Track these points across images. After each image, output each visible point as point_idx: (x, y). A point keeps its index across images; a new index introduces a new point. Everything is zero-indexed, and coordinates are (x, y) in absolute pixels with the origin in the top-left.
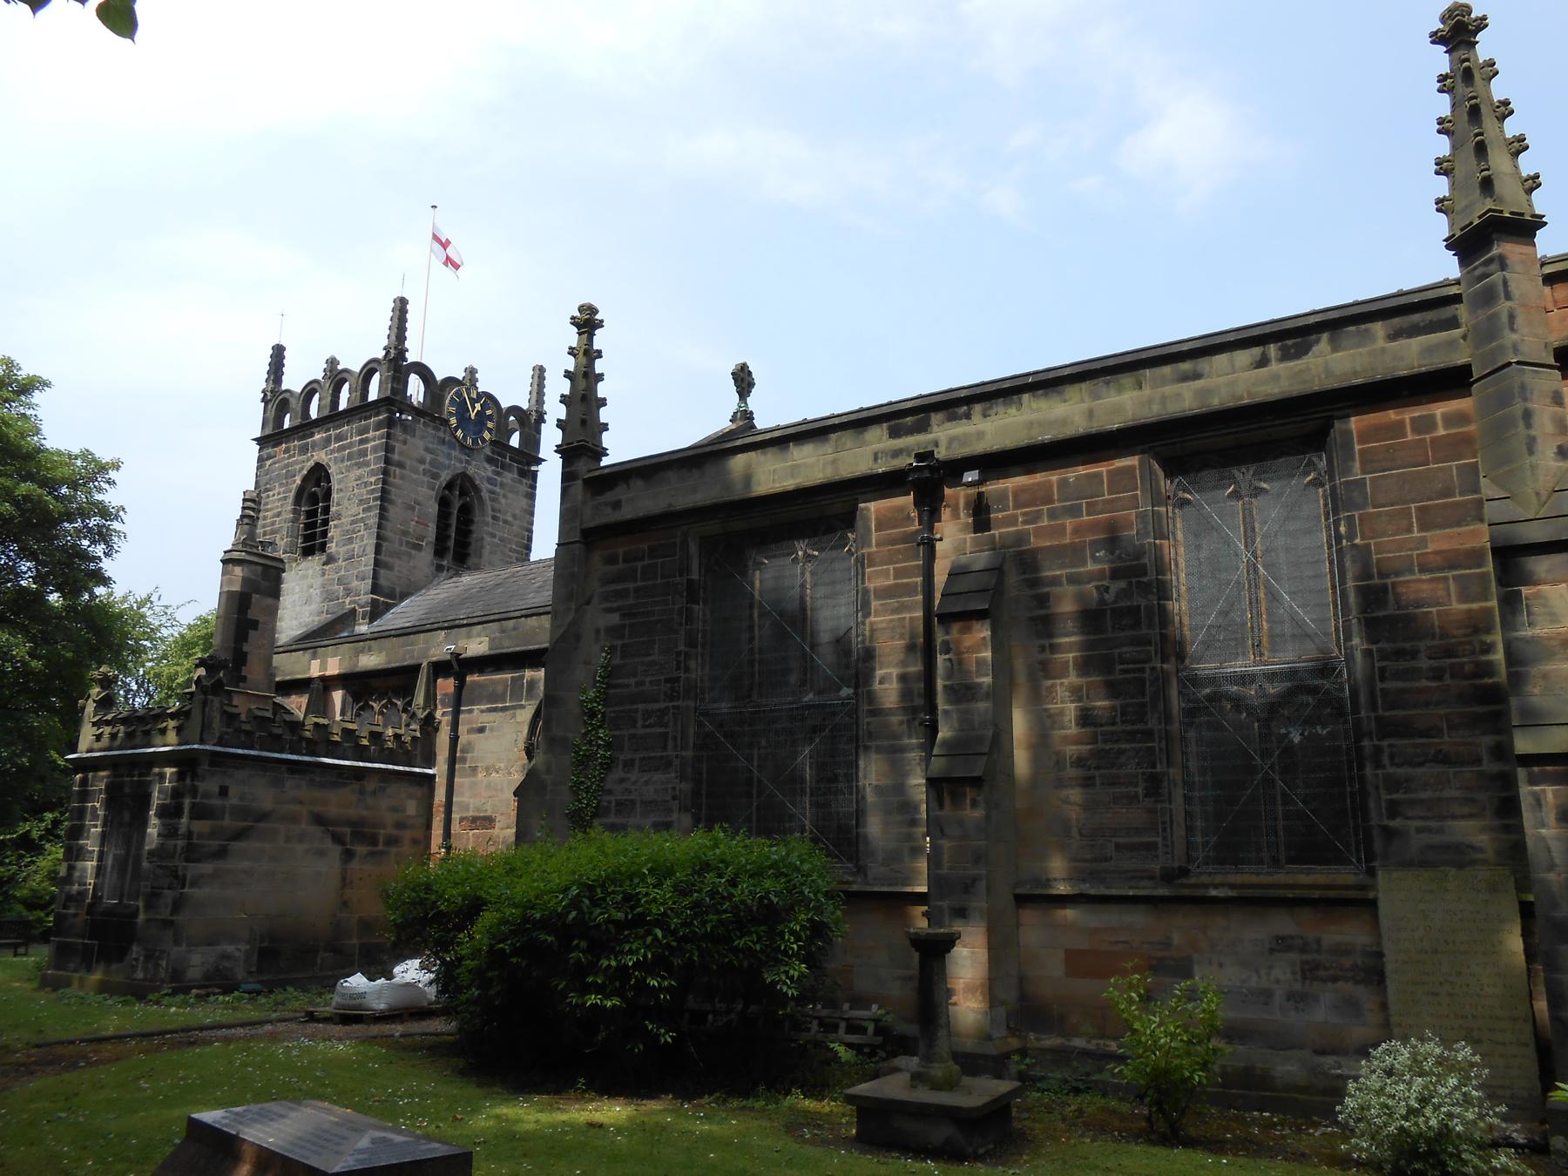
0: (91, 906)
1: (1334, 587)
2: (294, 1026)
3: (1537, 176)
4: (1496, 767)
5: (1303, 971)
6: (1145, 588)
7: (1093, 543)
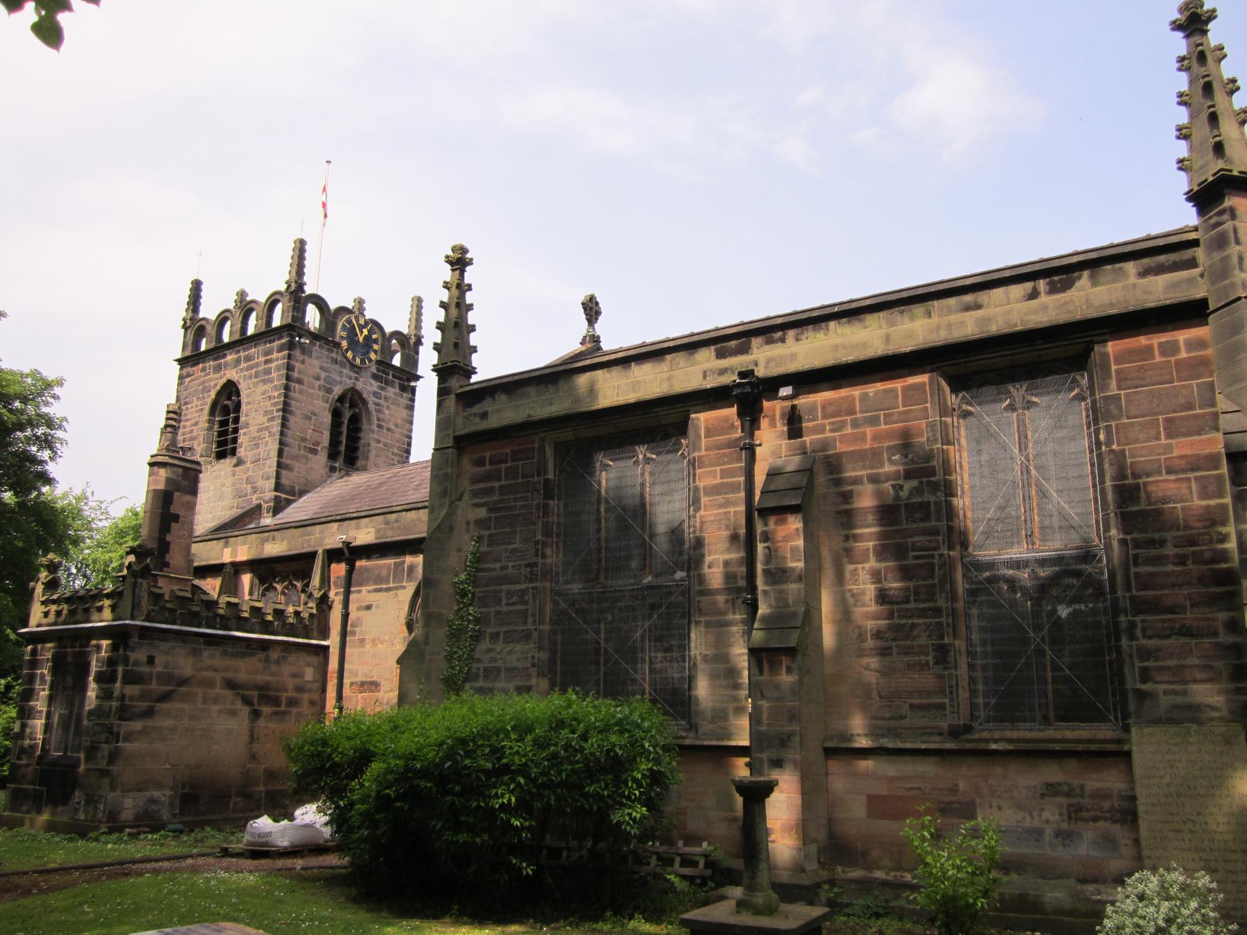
0: (40, 757)
1: (1094, 486)
2: (211, 860)
5: (1069, 812)
6: (934, 487)
7: (890, 448)
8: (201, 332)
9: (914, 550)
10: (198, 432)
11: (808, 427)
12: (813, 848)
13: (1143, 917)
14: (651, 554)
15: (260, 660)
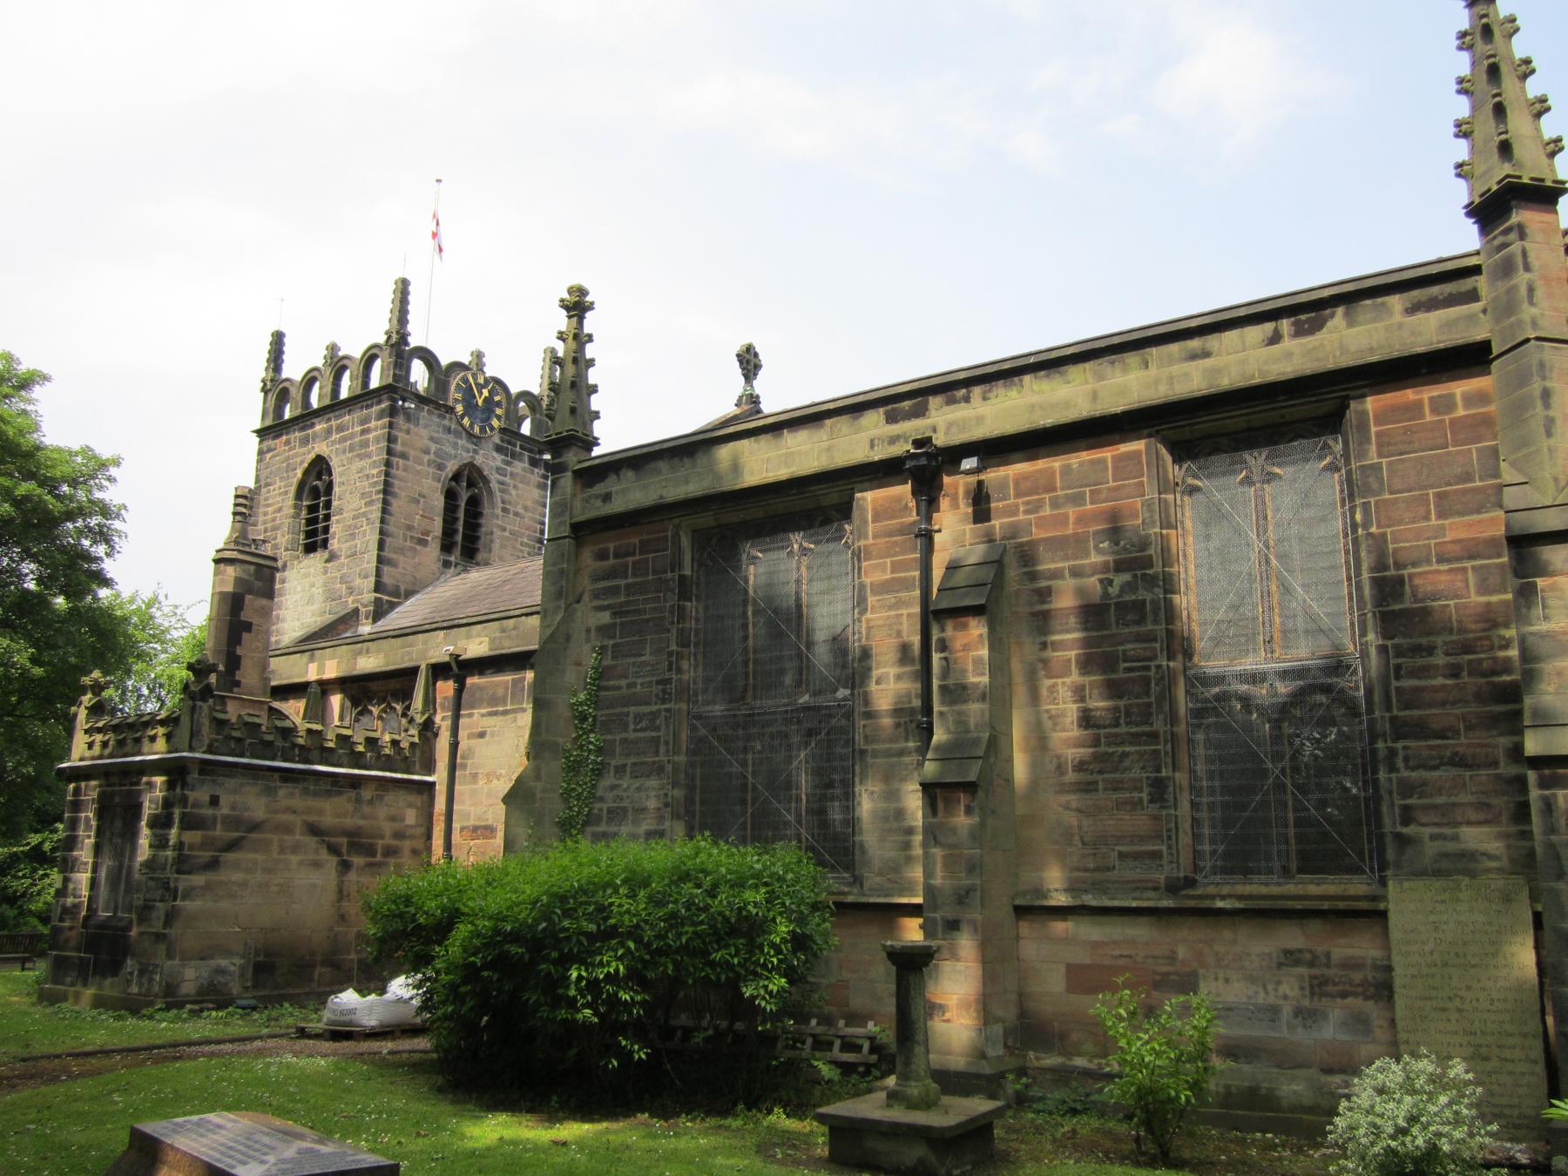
0: (86, 918)
1: (1349, 579)
2: (284, 1042)
3: (1559, 140)
4: (1514, 770)
5: (1311, 986)
6: (1151, 581)
7: (1096, 533)
8: (284, 396)
9: (1125, 661)
10: (280, 520)
11: (997, 508)
12: (998, 1029)
13: (1382, 1116)
14: (808, 668)
15: (349, 800)
